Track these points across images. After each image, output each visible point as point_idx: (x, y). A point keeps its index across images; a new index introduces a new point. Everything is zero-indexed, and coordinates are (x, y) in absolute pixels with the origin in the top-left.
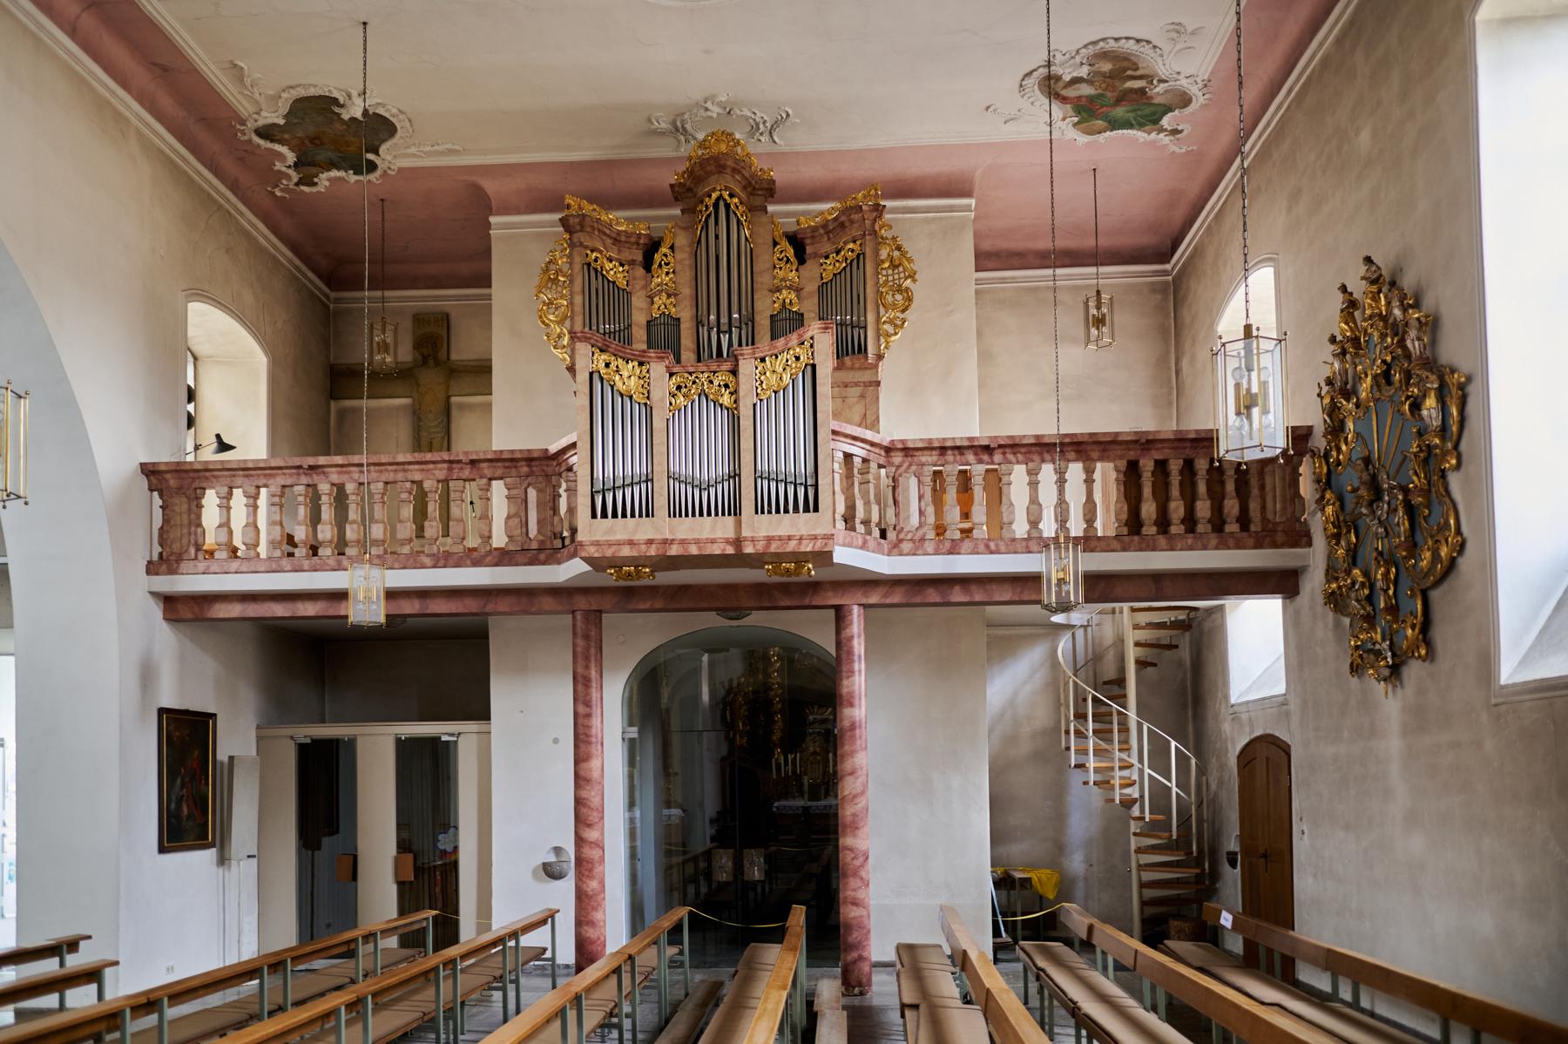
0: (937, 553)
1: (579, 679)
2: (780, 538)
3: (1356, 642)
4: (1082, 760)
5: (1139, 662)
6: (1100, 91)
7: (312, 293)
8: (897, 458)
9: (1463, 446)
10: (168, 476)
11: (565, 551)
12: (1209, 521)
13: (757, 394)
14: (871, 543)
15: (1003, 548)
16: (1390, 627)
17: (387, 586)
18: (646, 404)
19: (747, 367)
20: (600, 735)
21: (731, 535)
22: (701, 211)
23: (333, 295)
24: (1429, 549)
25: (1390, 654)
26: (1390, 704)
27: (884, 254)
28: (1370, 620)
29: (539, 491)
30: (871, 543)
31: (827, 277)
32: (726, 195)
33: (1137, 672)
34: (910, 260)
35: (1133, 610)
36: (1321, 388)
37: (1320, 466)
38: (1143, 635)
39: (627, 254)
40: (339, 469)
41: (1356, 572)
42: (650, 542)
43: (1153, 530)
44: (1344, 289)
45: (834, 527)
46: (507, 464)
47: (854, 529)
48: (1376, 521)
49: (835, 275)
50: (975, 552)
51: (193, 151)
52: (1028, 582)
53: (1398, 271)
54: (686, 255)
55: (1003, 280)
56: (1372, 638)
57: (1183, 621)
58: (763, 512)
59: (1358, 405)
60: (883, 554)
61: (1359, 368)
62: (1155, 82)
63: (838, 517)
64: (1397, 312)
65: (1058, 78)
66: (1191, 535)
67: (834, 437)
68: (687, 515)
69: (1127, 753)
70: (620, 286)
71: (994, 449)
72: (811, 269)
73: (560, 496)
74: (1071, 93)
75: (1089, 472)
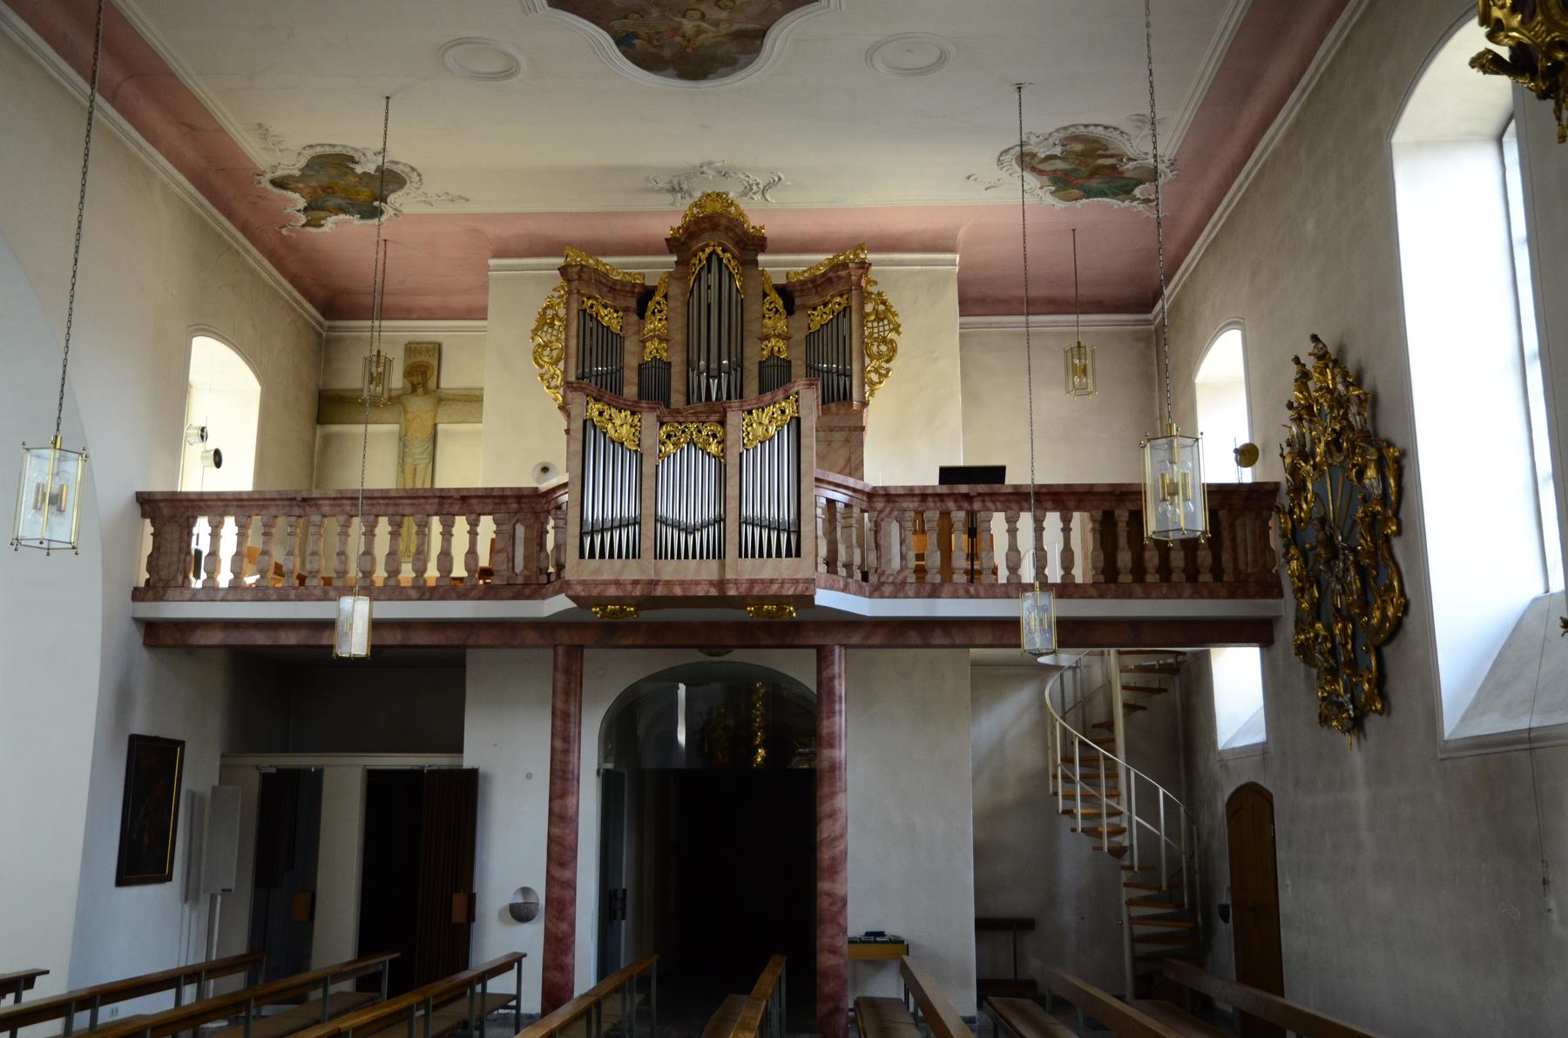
0: (918, 596)
1: (558, 713)
2: (763, 581)
3: (1322, 693)
4: (1069, 805)
5: (1126, 706)
6: (1073, 166)
7: (306, 322)
8: (880, 505)
9: (1402, 515)
10: (161, 505)
11: (550, 587)
12: (1184, 571)
13: (744, 444)
14: (853, 586)
15: (982, 593)
16: (1351, 680)
17: (374, 617)
18: (636, 451)
19: (733, 418)
20: (576, 772)
21: (715, 577)
22: (694, 264)
23: (327, 323)
24: (1378, 608)
25: (1351, 706)
26: (1356, 755)
27: (869, 308)
28: (1333, 673)
29: (527, 527)
30: (853, 586)
31: (815, 327)
32: (719, 250)
33: (1125, 715)
34: (895, 314)
35: (1120, 653)
36: (1282, 449)
37: (1286, 522)
38: (1131, 679)
39: (622, 301)
40: (332, 502)
41: (1319, 625)
42: (636, 582)
43: (1129, 578)
44: (1297, 360)
45: (816, 569)
46: (497, 501)
47: (836, 572)
48: (1334, 579)
49: (822, 326)
50: (955, 596)
51: (210, 199)
52: (1008, 629)
53: (1341, 350)
54: (679, 304)
55: (990, 325)
56: (1335, 690)
57: (1172, 664)
58: (746, 556)
59: (1315, 467)
60: (864, 596)
61: (1314, 433)
62: (1124, 160)
63: (820, 560)
64: (1340, 387)
65: (1033, 156)
66: (1165, 584)
67: (818, 484)
68: (672, 557)
69: (1116, 800)
70: (614, 330)
71: (974, 497)
72: (799, 319)
73: (548, 532)
74: (1047, 167)
75: (1066, 521)
